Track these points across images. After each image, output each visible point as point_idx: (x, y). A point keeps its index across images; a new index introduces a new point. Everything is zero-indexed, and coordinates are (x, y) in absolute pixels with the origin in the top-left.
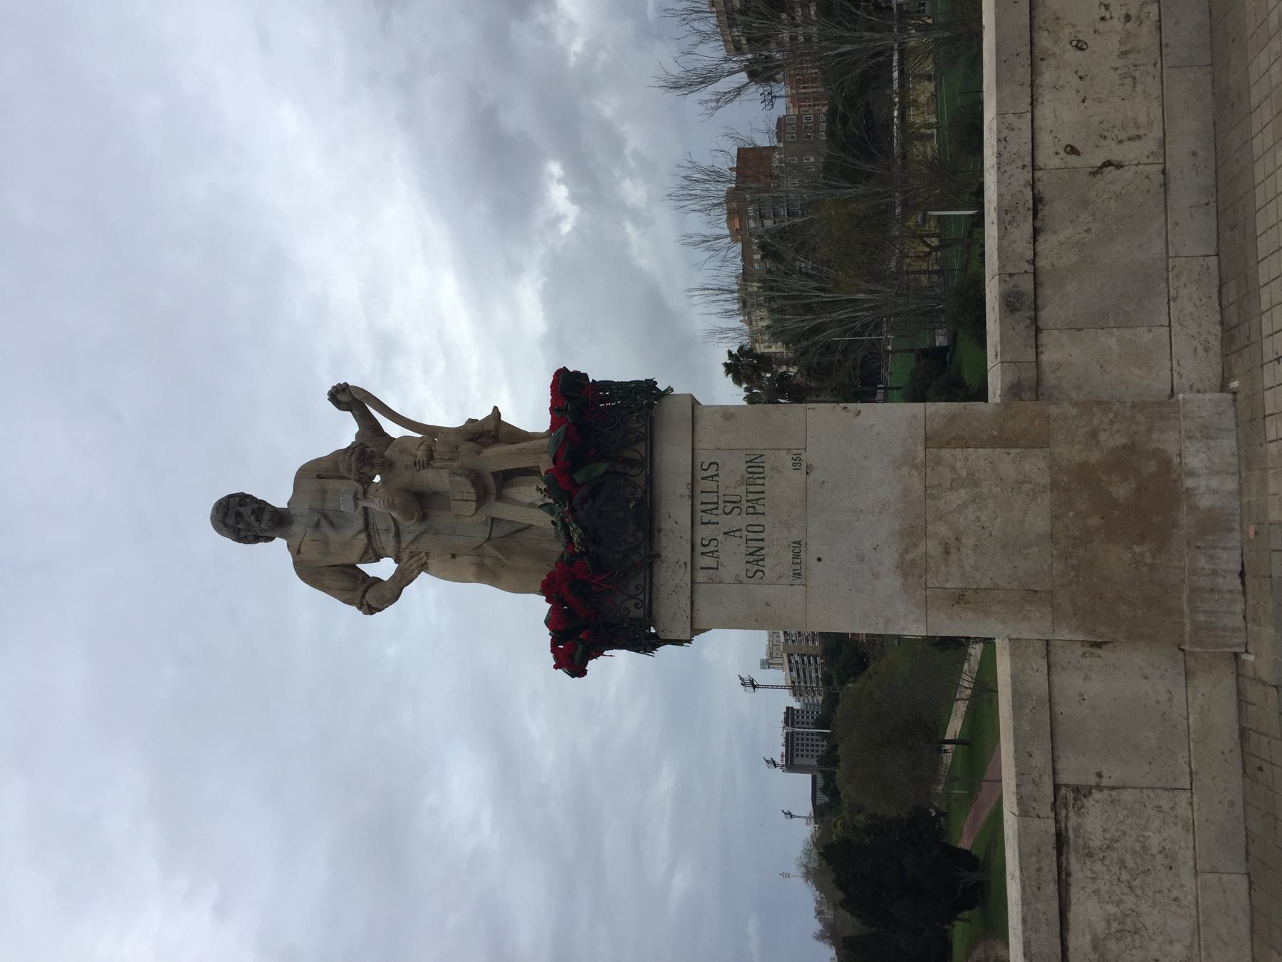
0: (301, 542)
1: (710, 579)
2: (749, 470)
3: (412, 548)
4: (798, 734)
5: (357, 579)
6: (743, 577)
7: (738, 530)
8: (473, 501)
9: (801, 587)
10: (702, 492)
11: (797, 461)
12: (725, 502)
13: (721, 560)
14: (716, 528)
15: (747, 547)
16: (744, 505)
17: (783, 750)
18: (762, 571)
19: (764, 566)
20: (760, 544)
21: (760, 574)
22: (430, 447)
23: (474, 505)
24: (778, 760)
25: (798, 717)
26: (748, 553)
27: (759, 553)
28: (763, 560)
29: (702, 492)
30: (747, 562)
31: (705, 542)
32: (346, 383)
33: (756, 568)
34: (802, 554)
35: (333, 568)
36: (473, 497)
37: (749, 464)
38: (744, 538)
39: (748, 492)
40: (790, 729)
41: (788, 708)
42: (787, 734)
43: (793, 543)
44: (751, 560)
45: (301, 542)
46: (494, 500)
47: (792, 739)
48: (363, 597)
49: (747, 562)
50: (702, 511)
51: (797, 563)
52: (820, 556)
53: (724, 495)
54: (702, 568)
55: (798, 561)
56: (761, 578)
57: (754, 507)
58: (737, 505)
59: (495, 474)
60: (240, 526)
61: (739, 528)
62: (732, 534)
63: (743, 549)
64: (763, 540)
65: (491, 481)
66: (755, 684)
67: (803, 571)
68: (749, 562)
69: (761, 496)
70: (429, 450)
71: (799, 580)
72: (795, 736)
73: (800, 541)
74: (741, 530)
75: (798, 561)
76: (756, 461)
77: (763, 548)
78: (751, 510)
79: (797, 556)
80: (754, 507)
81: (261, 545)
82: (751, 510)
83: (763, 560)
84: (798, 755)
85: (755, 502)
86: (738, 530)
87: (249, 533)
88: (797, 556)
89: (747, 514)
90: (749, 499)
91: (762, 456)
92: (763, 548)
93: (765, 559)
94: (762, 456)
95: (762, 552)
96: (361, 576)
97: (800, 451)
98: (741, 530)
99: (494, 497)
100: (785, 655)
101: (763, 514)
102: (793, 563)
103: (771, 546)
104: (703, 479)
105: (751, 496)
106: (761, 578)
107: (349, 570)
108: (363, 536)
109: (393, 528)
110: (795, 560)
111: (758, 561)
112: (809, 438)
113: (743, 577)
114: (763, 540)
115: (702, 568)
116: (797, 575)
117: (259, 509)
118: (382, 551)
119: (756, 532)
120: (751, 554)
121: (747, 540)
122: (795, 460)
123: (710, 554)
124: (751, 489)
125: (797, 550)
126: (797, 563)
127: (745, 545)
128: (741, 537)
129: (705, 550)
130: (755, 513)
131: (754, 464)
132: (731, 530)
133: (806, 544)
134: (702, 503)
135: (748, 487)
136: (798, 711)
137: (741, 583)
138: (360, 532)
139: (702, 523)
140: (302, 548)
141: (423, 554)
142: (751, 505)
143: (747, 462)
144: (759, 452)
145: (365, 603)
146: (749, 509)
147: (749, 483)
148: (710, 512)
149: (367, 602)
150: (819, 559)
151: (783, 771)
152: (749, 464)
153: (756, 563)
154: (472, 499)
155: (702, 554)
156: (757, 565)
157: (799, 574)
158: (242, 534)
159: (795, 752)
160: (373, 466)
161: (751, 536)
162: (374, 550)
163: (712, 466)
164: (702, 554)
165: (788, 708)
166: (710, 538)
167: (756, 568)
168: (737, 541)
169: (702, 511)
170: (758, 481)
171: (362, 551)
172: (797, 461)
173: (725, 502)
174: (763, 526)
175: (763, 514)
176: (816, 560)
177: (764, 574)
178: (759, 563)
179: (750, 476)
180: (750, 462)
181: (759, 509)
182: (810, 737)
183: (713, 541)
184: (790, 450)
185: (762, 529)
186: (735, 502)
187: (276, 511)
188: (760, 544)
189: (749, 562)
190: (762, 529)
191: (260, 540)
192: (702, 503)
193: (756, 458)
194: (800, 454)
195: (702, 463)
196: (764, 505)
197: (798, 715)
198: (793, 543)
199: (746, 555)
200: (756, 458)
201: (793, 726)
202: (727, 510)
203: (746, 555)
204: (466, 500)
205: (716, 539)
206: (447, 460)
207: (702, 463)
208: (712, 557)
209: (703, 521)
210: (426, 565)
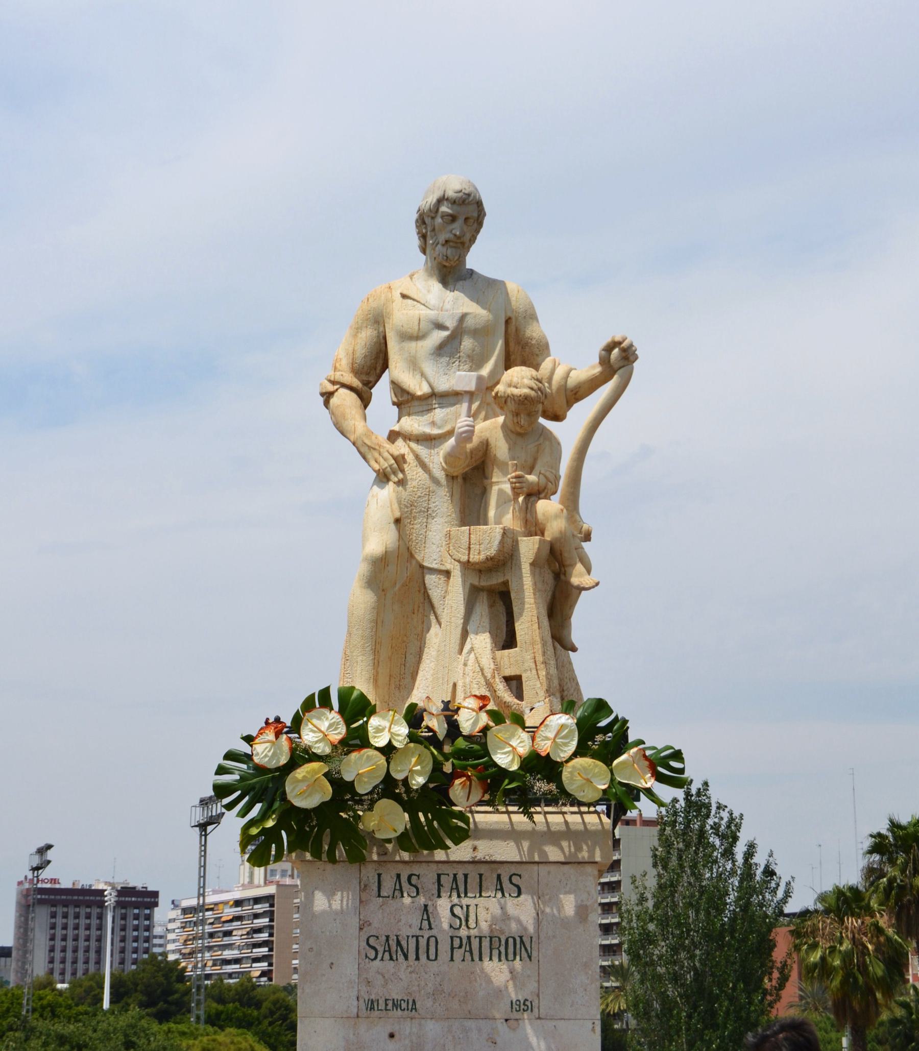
0: (418, 301)
1: (365, 886)
2: (511, 941)
3: (410, 458)
4: (101, 917)
5: (368, 374)
6: (368, 931)
7: (430, 924)
8: (469, 558)
9: (355, 1010)
10: (481, 875)
11: (522, 1007)
12: (468, 906)
13: (391, 901)
14: (433, 895)
15: (408, 937)
16: (463, 932)
17: (66, 884)
18: (376, 958)
19: (382, 959)
20: (412, 955)
21: (372, 954)
22: (543, 490)
23: (464, 558)
24: (46, 874)
25: (136, 917)
26: (400, 938)
27: (400, 952)
28: (391, 959)
29: (481, 875)
30: (388, 937)
31: (414, 880)
32: (636, 358)
33: (380, 949)
34: (399, 1012)
35: (383, 341)
36: (475, 558)
37: (518, 940)
38: (419, 933)
39: (480, 938)
40: (110, 899)
41: (155, 894)
42: (101, 892)
43: (414, 1001)
44: (391, 942)
45: (418, 301)
46: (472, 582)
47: (89, 905)
48: (344, 385)
49: (388, 937)
50: (455, 875)
51: (386, 1005)
52: (393, 1040)
53: (477, 905)
54: (379, 875)
55: (390, 1006)
56: (366, 956)
57: (460, 947)
58: (464, 923)
59: (506, 583)
60: (439, 220)
61: (433, 926)
62: (425, 917)
63: (405, 932)
64: (417, 958)
65: (495, 580)
66: (209, 828)
67: (376, 1013)
68: (387, 940)
69: (476, 958)
70: (538, 490)
71: (364, 1008)
72: (95, 911)
73: (416, 1009)
74: (430, 928)
75: (390, 1006)
76: (523, 949)
77: (406, 958)
78: (457, 942)
79: (396, 1005)
80: (460, 947)
81: (415, 241)
82: (457, 942)
83: (391, 959)
84: (53, 915)
85: (468, 949)
86: (430, 924)
87: (429, 229)
88: (396, 1005)
89: (452, 938)
90: (406, 1008)
91: (530, 957)
92: (406, 958)
93: (392, 962)
94: (530, 957)
95: (401, 958)
96: (371, 379)
97: (536, 1010)
98: (430, 928)
99: (476, 583)
100: (271, 890)
101: (452, 959)
102: (386, 1000)
103: (410, 969)
104: (499, 876)
105: (475, 943)
106: (366, 956)
107: (381, 362)
108: (424, 389)
109: (436, 431)
110: (390, 1003)
111: (390, 951)
112: (553, 1023)
113: (368, 931)
114: (417, 958)
115: (379, 875)
116: (372, 1005)
117: (463, 244)
118: (405, 411)
119: (428, 949)
120: (399, 943)
121: (417, 937)
122: (524, 1004)
123: (398, 887)
124: (486, 943)
125: (404, 1005)
126: (386, 1005)
127: (410, 934)
128: (421, 929)
129: (404, 879)
130: (452, 949)
131: (518, 946)
132: (430, 915)
133: (412, 1019)
134: (466, 876)
135: (488, 939)
136: (149, 917)
137: (361, 929)
138: (431, 386)
139: (439, 876)
140: (409, 301)
141: (401, 476)
142: (464, 941)
143: (521, 937)
144: (534, 954)
145: (336, 387)
146: (458, 940)
147: (493, 939)
148: (454, 886)
149: (337, 390)
150: (392, 1036)
151: (20, 883)
152: (518, 940)
153: (387, 949)
154: (471, 556)
155: (398, 876)
156: (385, 951)
157: (372, 1008)
158: (428, 220)
159: (60, 910)
160: (517, 414)
161: (423, 942)
162: (407, 402)
163: (516, 889)
164: (398, 876)
165: (155, 894)
166: (419, 886)
167: (380, 949)
168: (416, 922)
169: (455, 875)
170: (495, 952)
171: (405, 387)
172: (522, 1007)
173: (468, 906)
174: (436, 959)
175: (452, 959)
176: (391, 1031)
177: (372, 960)
178: (387, 954)
179: (503, 942)
180: (522, 942)
181: (458, 954)
182: (94, 933)
183: (415, 890)
184: (538, 996)
185: (432, 957)
186: (467, 921)
187: (461, 260)
188: (412, 955)
189: (387, 940)
190: (432, 957)
191: (422, 239)
192: (466, 876)
193: (526, 949)
194: (532, 1010)
195: (520, 876)
196: (463, 960)
197: (141, 928)
198: (414, 1001)
199: (397, 936)
200: (526, 949)
201: (119, 904)
202: (457, 910)
203: (397, 936)
204: (469, 548)
205: (418, 893)
206: (526, 517)
207: (520, 876)
208: (395, 889)
209: (442, 876)
210: (385, 480)
